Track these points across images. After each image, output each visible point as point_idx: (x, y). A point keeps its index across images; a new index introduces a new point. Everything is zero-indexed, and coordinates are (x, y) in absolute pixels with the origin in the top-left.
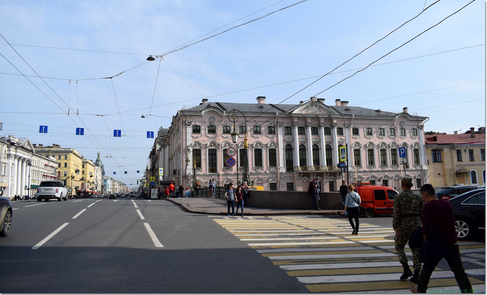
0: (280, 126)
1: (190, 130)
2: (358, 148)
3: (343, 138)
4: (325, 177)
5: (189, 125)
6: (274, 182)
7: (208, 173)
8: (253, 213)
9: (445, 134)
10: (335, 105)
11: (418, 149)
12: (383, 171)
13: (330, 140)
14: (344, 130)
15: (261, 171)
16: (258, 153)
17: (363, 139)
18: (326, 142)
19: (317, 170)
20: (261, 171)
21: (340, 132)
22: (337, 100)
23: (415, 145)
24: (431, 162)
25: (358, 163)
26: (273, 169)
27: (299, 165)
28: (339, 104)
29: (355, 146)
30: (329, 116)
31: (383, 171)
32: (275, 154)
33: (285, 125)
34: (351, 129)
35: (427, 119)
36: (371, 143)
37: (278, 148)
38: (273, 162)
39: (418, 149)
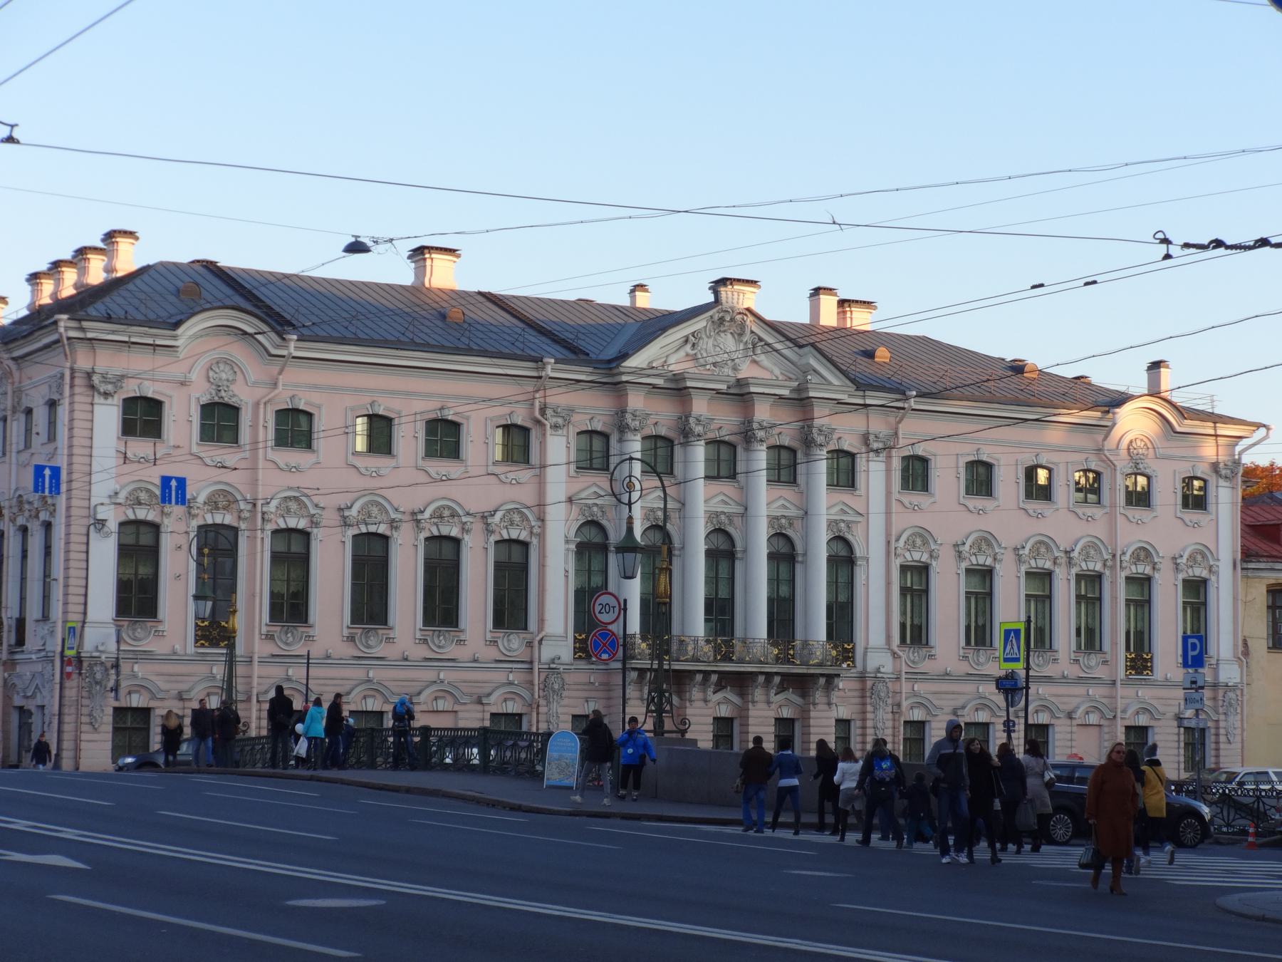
0: (556, 427)
1: (108, 417)
2: (920, 556)
3: (857, 504)
4: (758, 694)
5: (106, 395)
6: (512, 708)
7: (191, 649)
8: (666, 813)
9: (1017, 368)
10: (804, 318)
11: (1204, 582)
12: (1080, 680)
13: (793, 512)
14: (861, 463)
15: (451, 651)
16: (371, 561)
17: (946, 512)
18: (773, 520)
19: (727, 658)
20: (451, 651)
21: (845, 473)
22: (817, 291)
23: (1192, 557)
24: (1260, 644)
25: (916, 633)
26: (514, 643)
27: (822, 634)
28: (828, 307)
29: (911, 545)
30: (799, 390)
31: (1080, 680)
32: (524, 567)
33: (582, 422)
34: (896, 464)
35: (1262, 431)
36: (986, 541)
37: (542, 536)
38: (511, 608)
39: (1204, 582)
